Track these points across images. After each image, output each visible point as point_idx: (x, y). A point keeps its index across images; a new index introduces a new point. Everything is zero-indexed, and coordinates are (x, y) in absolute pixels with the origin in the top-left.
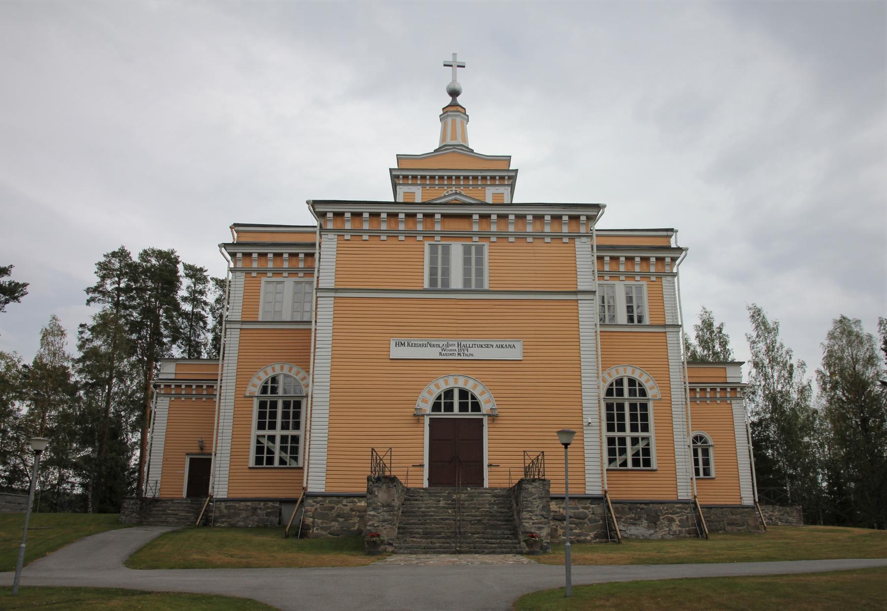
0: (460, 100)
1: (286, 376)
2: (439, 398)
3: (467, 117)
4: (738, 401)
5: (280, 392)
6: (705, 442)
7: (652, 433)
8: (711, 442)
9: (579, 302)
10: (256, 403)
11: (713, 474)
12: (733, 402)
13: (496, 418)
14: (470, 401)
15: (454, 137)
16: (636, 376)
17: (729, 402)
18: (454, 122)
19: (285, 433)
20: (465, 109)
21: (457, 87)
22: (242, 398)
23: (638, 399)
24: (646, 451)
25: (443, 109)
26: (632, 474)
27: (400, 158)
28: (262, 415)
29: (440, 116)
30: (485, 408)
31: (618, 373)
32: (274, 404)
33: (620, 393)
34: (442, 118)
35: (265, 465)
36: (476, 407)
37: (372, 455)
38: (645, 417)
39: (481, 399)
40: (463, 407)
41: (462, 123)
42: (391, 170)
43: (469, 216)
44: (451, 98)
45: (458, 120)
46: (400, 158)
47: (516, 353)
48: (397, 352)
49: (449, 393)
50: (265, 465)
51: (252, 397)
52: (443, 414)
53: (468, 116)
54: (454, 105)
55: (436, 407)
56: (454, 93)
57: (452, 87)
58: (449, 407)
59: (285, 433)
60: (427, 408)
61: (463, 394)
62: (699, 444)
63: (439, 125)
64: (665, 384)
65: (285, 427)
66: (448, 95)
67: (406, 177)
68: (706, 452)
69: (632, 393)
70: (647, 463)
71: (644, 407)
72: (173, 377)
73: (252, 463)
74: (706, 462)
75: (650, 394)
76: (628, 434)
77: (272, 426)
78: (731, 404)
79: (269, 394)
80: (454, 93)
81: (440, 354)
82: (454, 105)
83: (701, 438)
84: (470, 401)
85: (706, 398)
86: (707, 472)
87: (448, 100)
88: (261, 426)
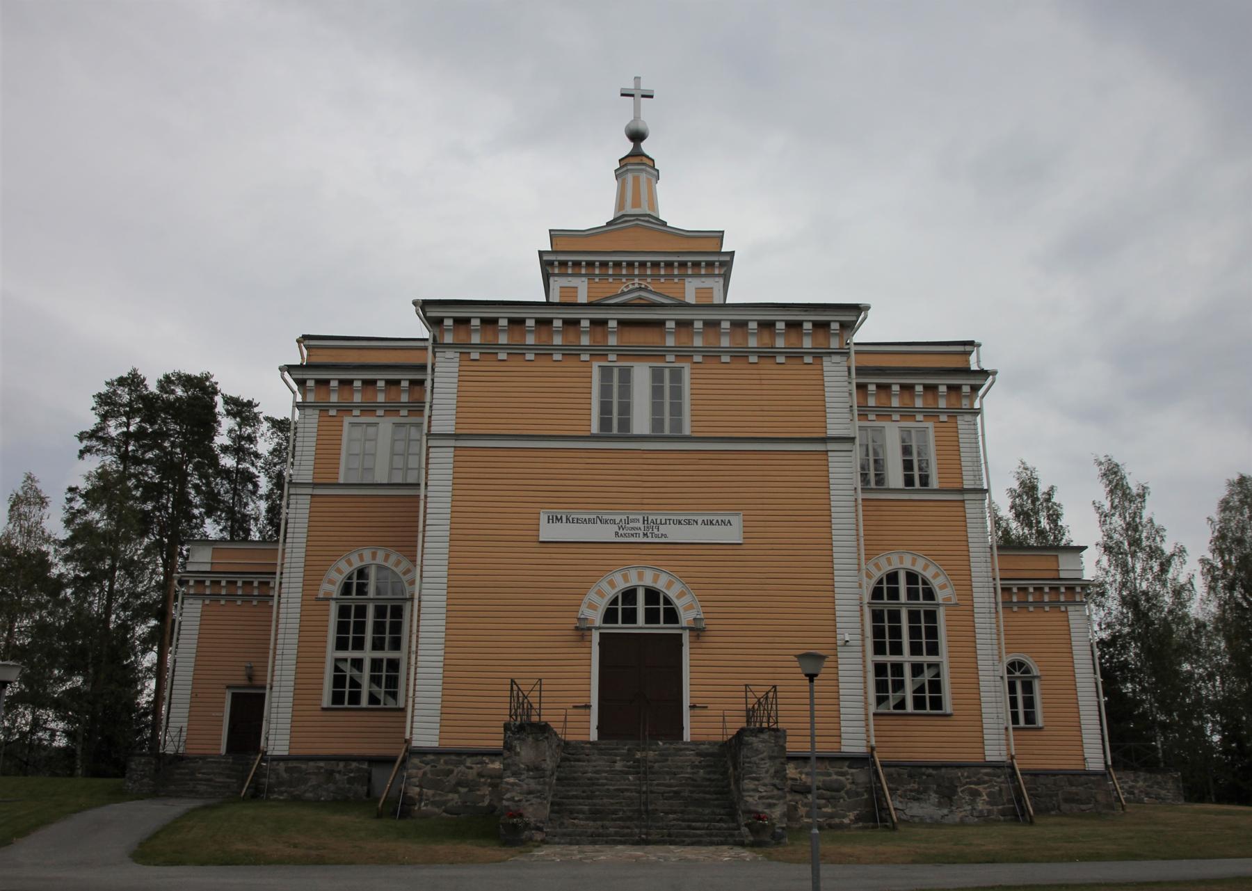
0: (645, 146)
1: (380, 568)
2: (615, 601)
3: (656, 173)
4: (1078, 608)
5: (371, 592)
6: (1028, 671)
7: (943, 658)
8: (1035, 672)
9: (830, 454)
10: (334, 608)
11: (1040, 722)
12: (1070, 608)
13: (702, 634)
14: (662, 606)
15: (636, 203)
16: (918, 568)
17: (1063, 609)
18: (636, 179)
19: (378, 654)
20: (653, 161)
21: (641, 127)
22: (313, 601)
23: (921, 604)
24: (936, 686)
25: (620, 161)
26: (912, 721)
27: (554, 235)
28: (342, 627)
29: (616, 171)
30: (686, 618)
31: (890, 564)
32: (361, 611)
33: (894, 594)
34: (619, 174)
35: (346, 705)
36: (672, 616)
37: (512, 690)
38: (933, 633)
39: (679, 604)
40: (652, 617)
41: (649, 181)
42: (541, 253)
43: (661, 324)
44: (632, 144)
45: (643, 176)
46: (554, 235)
47: (732, 532)
48: (549, 532)
49: (630, 595)
50: (346, 705)
51: (328, 599)
52: (620, 628)
53: (658, 171)
54: (637, 154)
55: (610, 616)
56: (637, 137)
57: (633, 127)
58: (630, 617)
59: (378, 654)
60: (597, 617)
61: (652, 595)
62: (1018, 674)
63: (613, 185)
64: (964, 582)
65: (378, 645)
66: (627, 140)
67: (563, 264)
68: (1028, 687)
69: (912, 594)
70: (937, 703)
71: (931, 616)
72: (207, 568)
73: (326, 701)
74: (1029, 703)
75: (940, 596)
76: (906, 658)
77: (359, 645)
78: (1066, 611)
79: (354, 596)
80: (637, 137)
81: (617, 534)
82: (637, 154)
83: (1021, 664)
84: (662, 606)
85: (1027, 602)
86: (1030, 718)
87: (628, 147)
88: (341, 644)
